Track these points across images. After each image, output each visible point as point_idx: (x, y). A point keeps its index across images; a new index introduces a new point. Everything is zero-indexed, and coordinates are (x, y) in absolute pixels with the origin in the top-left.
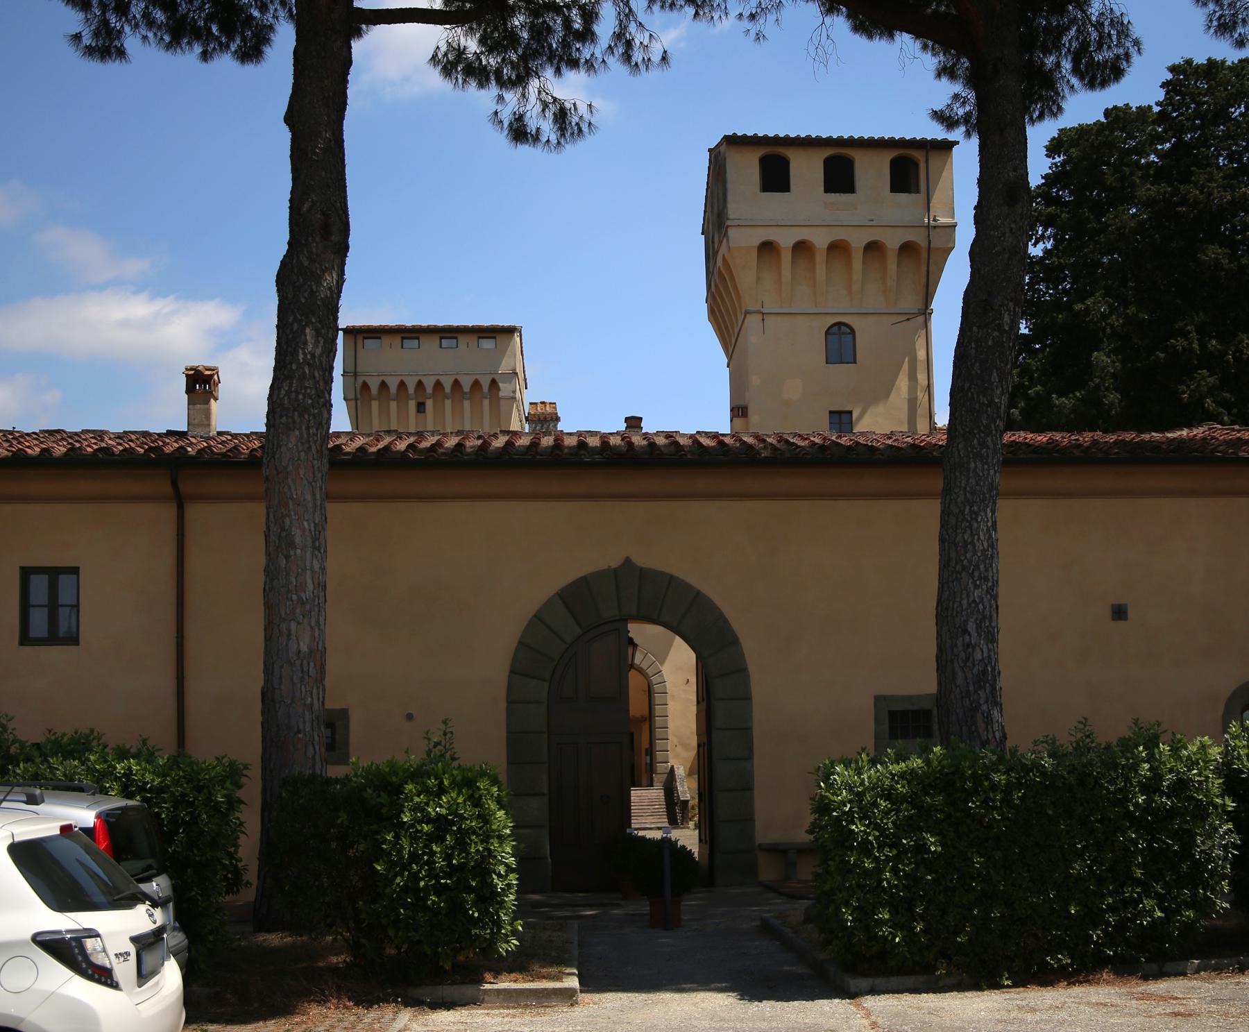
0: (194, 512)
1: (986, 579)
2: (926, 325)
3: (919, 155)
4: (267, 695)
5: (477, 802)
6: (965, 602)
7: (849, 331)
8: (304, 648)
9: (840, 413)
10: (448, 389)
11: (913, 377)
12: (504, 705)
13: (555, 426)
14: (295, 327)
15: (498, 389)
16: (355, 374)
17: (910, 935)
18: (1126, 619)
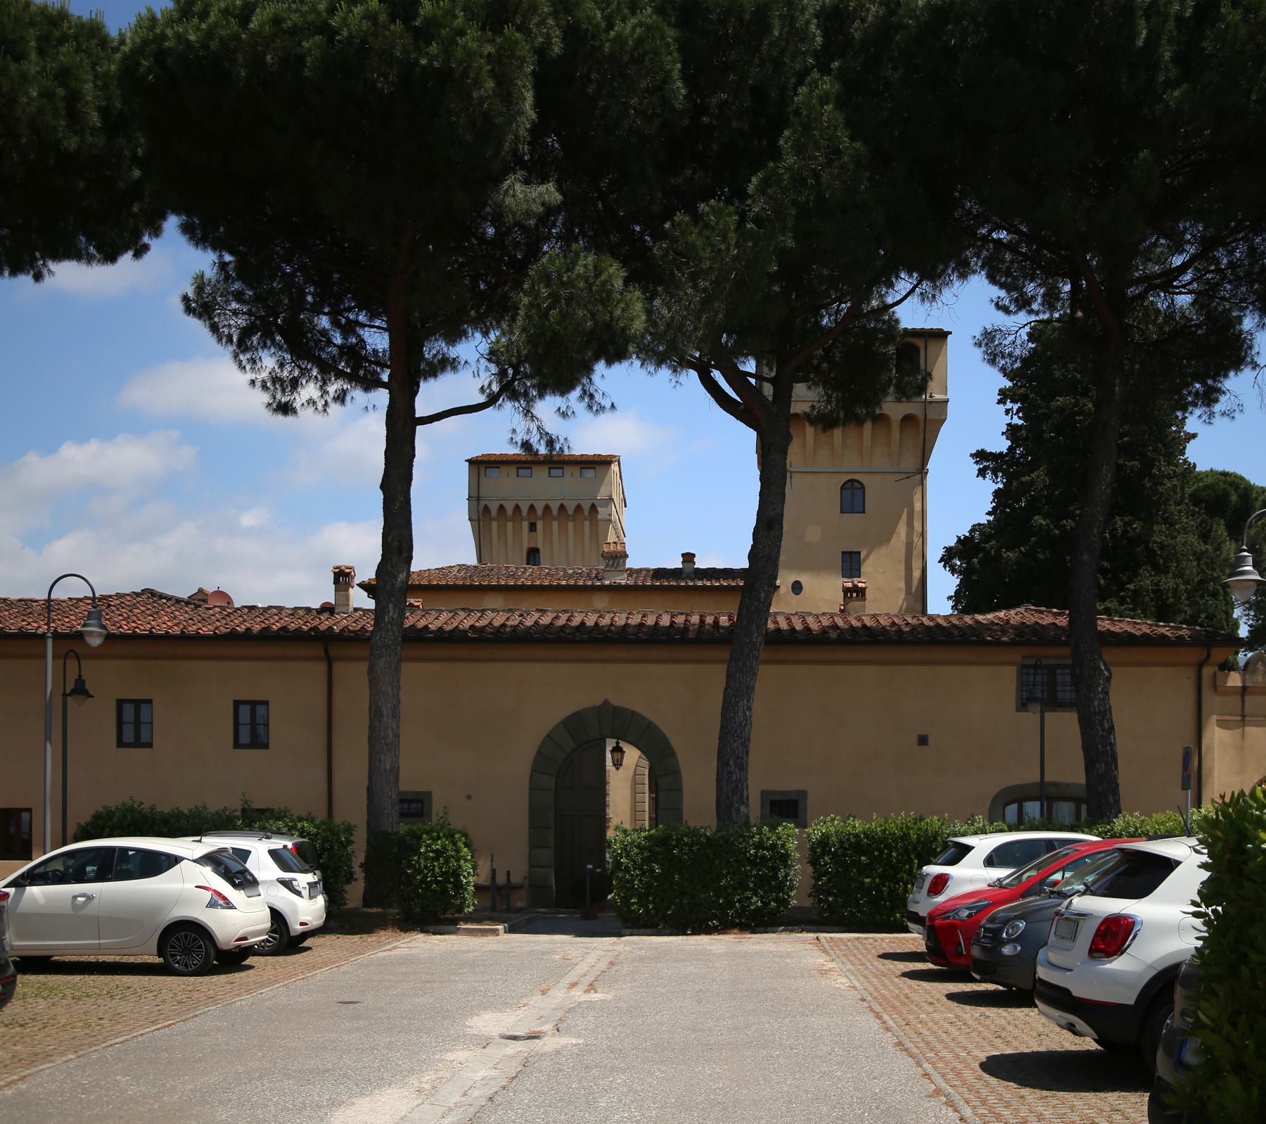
0: (338, 667)
1: (741, 737)
2: (922, 483)
3: (919, 343)
4: (370, 791)
5: (455, 844)
6: (728, 749)
7: (860, 486)
8: (388, 767)
9: (851, 553)
10: (555, 512)
11: (910, 525)
12: (528, 791)
13: (624, 562)
14: (384, 603)
15: (597, 512)
16: (478, 499)
17: (647, 910)
18: (927, 744)
